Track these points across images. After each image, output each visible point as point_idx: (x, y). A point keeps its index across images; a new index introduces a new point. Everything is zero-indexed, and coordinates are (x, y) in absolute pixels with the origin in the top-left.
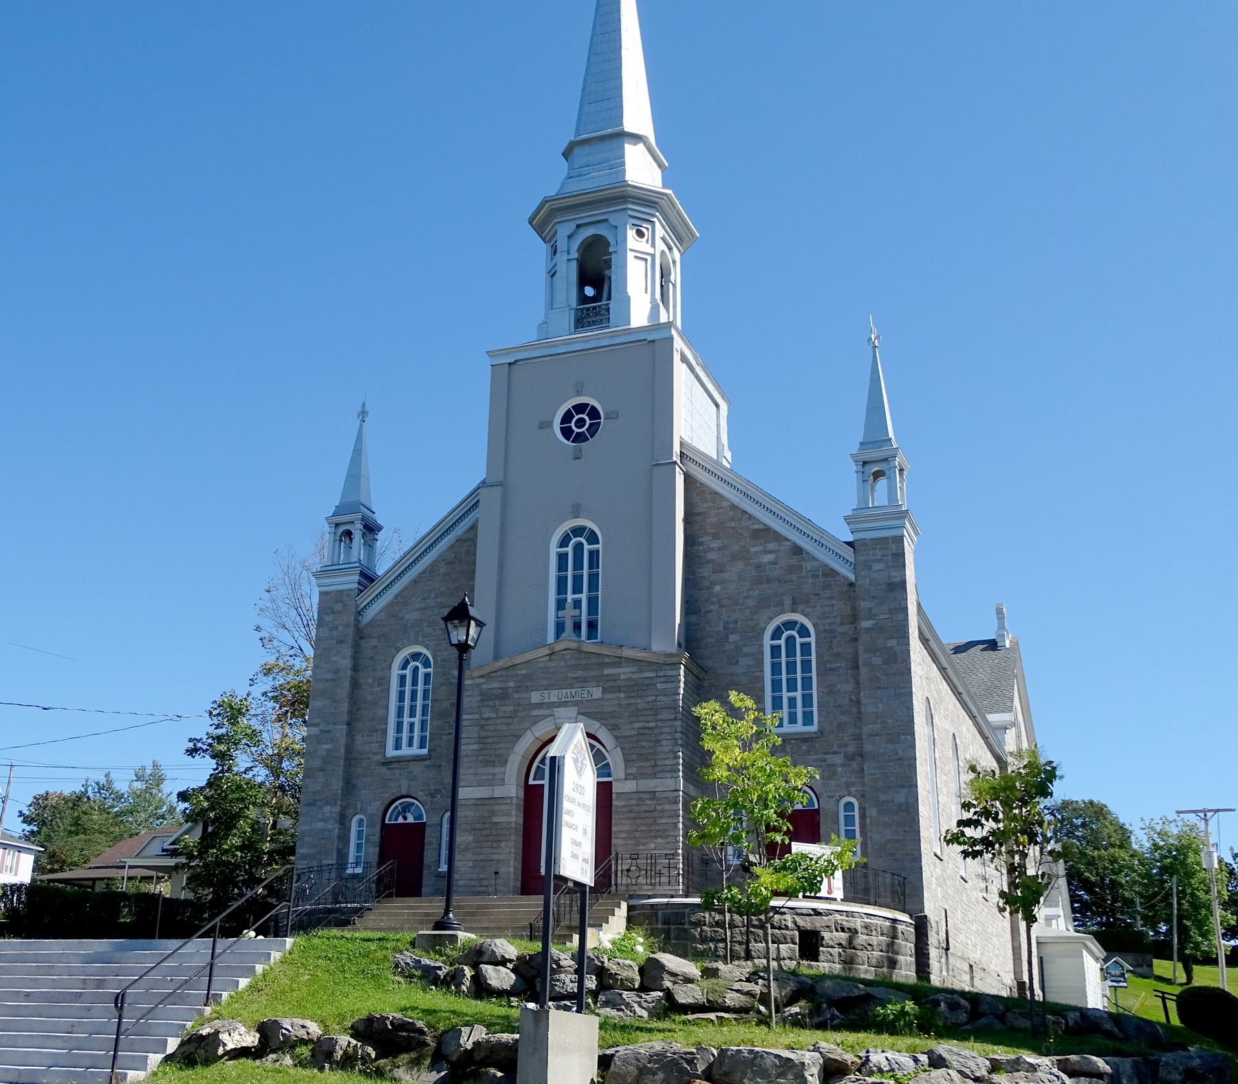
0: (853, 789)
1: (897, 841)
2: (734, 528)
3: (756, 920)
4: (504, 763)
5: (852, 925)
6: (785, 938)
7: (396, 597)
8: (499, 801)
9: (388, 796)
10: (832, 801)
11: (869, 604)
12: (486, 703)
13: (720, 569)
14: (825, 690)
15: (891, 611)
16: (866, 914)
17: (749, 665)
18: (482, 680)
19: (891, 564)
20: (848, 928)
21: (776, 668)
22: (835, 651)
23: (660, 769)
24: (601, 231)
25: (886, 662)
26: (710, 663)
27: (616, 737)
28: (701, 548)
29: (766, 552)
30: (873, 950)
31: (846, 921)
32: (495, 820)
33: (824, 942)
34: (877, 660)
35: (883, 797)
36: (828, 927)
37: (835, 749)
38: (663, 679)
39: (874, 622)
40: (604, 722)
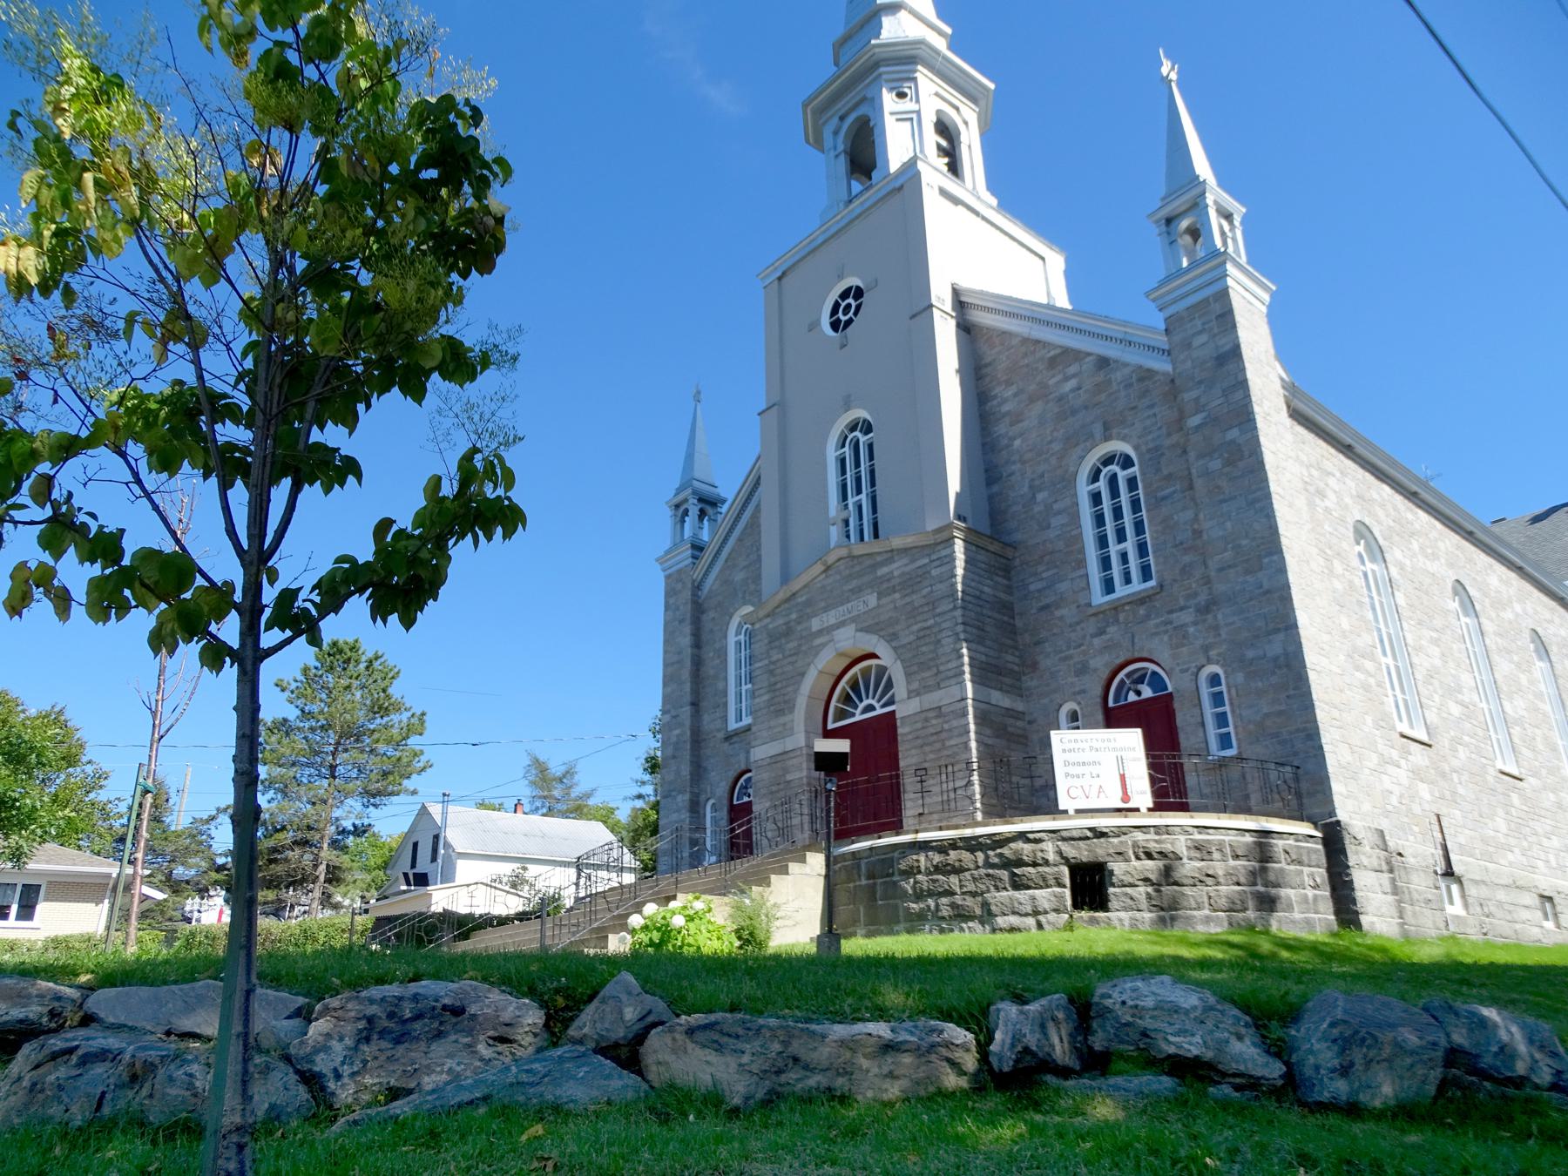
0: (1213, 653)
1: (1280, 713)
2: (1027, 365)
3: (996, 855)
4: (792, 709)
5: (1168, 847)
6: (1044, 879)
7: (726, 561)
8: (792, 755)
9: (732, 774)
10: (1187, 677)
11: (1194, 394)
12: (773, 645)
13: (1017, 418)
14: (1160, 528)
15: (1226, 393)
16: (1197, 827)
17: (1063, 525)
18: (768, 620)
19: (1216, 331)
20: (1160, 853)
21: (1099, 520)
22: (1165, 472)
23: (942, 676)
24: (862, 110)
25: (1230, 462)
26: (1018, 537)
27: (895, 649)
28: (995, 402)
29: (1067, 379)
30: (1218, 884)
31: (1156, 841)
32: (789, 777)
33: (1115, 880)
34: (1216, 464)
35: (1250, 654)
36: (1120, 854)
37: (1182, 602)
38: (938, 563)
39: (1204, 414)
40: (882, 633)
